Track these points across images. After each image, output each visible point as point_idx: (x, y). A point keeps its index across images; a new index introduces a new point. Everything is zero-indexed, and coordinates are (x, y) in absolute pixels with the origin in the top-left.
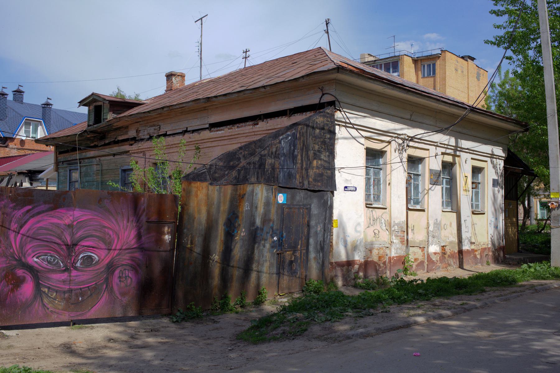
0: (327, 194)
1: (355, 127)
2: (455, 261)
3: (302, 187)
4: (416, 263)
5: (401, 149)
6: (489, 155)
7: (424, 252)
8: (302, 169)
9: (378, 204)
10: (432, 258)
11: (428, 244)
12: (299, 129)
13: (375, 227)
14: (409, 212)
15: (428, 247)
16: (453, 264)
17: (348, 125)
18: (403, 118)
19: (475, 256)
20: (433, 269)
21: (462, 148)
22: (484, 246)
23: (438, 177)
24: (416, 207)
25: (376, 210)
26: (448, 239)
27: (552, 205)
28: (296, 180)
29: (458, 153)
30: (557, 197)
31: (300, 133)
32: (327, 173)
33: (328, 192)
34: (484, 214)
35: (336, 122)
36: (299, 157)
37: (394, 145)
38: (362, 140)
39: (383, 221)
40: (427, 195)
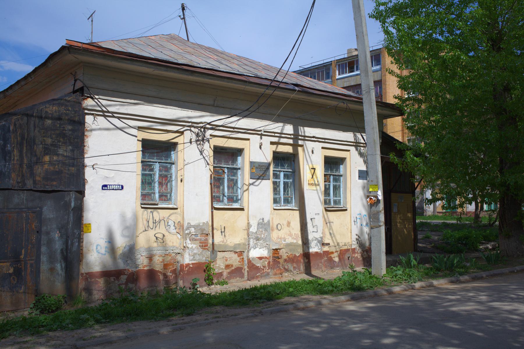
0: (69, 194)
1: (115, 115)
2: (295, 265)
3: (22, 187)
4: (228, 271)
5: (201, 139)
6: (352, 144)
7: (242, 257)
8: (21, 165)
9: (167, 203)
10: (254, 263)
11: (249, 247)
12: (13, 121)
13: (157, 230)
14: (215, 211)
15: (248, 252)
16: (292, 269)
17: (95, 113)
18: (202, 104)
19: (330, 260)
20: (257, 277)
21: (305, 136)
22: (346, 248)
23: (265, 171)
24: (231, 205)
25: (159, 210)
26: (285, 241)
27: (370, 200)
28: (9, 179)
29: (300, 142)
30: (376, 190)
31: (15, 125)
32: (69, 169)
33: (71, 192)
34: (346, 210)
35: (86, 111)
36: (15, 153)
37: (188, 135)
38: (134, 132)
39: (171, 223)
40: (247, 192)
